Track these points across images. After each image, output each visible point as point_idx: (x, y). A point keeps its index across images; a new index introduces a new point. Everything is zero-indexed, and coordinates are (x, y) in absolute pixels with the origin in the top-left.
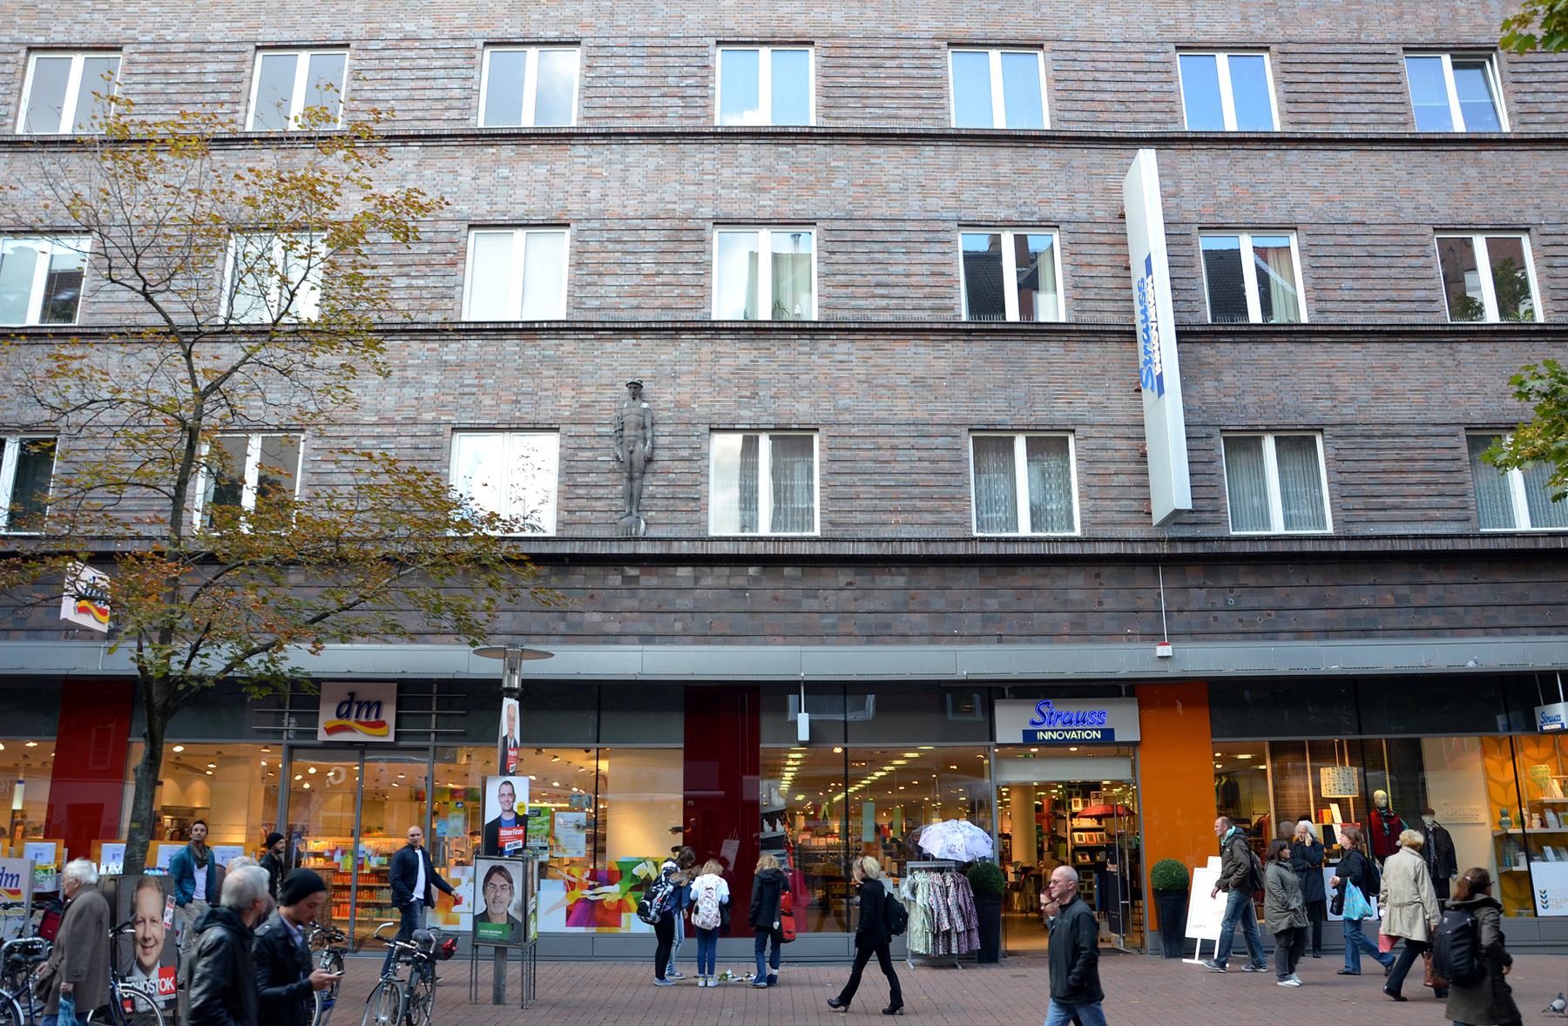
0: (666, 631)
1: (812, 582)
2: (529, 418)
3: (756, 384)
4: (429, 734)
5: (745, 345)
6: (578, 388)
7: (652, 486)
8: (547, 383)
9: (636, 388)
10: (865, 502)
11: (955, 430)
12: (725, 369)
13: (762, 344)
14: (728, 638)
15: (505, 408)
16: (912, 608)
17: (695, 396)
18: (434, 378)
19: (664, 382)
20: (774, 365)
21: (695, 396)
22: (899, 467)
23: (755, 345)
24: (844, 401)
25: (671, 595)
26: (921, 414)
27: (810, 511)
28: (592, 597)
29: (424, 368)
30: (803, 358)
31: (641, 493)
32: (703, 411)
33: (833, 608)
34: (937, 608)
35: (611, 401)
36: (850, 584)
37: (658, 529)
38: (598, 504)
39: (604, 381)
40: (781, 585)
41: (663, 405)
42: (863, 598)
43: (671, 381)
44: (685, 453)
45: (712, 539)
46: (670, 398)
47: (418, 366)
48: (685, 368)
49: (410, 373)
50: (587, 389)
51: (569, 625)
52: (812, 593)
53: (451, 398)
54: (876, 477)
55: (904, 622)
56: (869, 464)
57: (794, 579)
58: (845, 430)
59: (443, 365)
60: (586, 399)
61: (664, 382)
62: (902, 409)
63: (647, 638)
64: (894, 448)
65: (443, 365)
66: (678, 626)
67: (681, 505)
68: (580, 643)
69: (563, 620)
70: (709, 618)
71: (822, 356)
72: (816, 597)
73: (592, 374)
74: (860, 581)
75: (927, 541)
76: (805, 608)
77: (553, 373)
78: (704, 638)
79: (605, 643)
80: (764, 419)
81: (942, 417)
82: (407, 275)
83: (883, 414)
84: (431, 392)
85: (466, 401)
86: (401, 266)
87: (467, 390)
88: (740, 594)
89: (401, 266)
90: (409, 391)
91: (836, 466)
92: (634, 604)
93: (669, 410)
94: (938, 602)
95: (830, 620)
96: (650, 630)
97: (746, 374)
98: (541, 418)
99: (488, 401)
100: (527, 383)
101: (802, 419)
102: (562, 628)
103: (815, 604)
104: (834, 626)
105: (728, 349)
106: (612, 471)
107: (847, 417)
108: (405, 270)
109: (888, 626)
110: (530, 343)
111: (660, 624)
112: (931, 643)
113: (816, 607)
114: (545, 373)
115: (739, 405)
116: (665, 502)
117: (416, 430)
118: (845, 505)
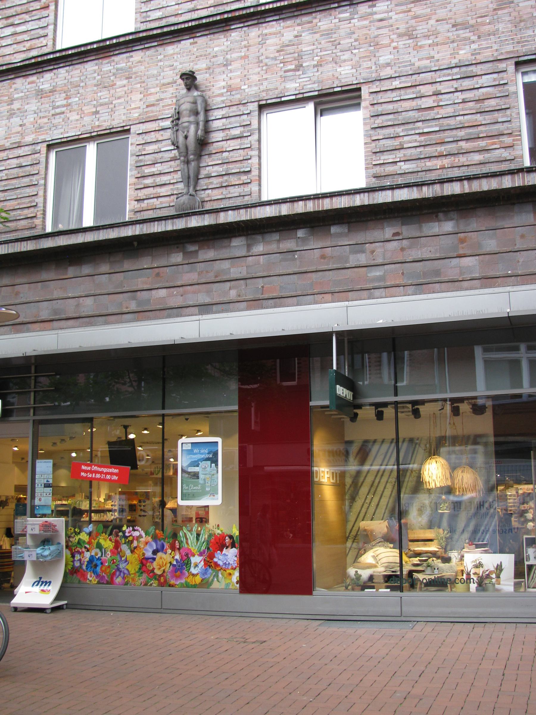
0: (222, 299)
1: (360, 237)
2: (106, 125)
3: (300, 57)
4: (28, 409)
5: (289, 23)
6: (145, 93)
7: (211, 166)
8: (120, 92)
9: (189, 79)
10: (409, 152)
11: (502, 66)
12: (272, 48)
13: (305, 19)
14: (278, 300)
15: (87, 119)
16: (461, 252)
17: (245, 78)
18: (33, 106)
19: (217, 70)
20: (317, 36)
21: (245, 78)
22: (443, 112)
23: (298, 21)
24: (385, 57)
25: (226, 265)
26: (464, 54)
27: (295, 374)
28: (158, 275)
29: (25, 99)
30: (345, 26)
31: (198, 173)
32: (254, 90)
33: (380, 261)
34: (488, 250)
35: (171, 95)
36: (397, 234)
37: (221, 198)
38: (163, 191)
39: (166, 81)
40: (328, 244)
41: (218, 92)
42: (410, 248)
43: (223, 69)
44: (236, 132)
45: (269, 203)
46: (223, 84)
47: (21, 98)
48: (235, 55)
49: (16, 105)
50: (153, 90)
51: (139, 304)
52: (358, 248)
53: (46, 120)
54: (419, 124)
55: (453, 268)
56: (411, 114)
57: (340, 235)
58: (387, 85)
59: (40, 94)
60: (152, 99)
61: (217, 70)
62: (444, 56)
63: (205, 308)
64: (437, 94)
65: (40, 94)
66: (233, 294)
67: (234, 180)
68: (149, 319)
69: (134, 298)
70: (260, 283)
71: (362, 18)
72: (363, 251)
73: (156, 77)
74: (407, 230)
75: (469, 178)
76: (351, 264)
77: (125, 82)
78: (256, 302)
79: (169, 316)
80: (309, 87)
81: (487, 55)
82: (13, 25)
83: (426, 63)
84: (31, 118)
85: (58, 120)
86: (8, 18)
87: (58, 111)
88: (289, 256)
89: (8, 18)
90: (16, 121)
91: (379, 121)
92: (193, 277)
93: (222, 95)
94: (491, 244)
95: (377, 273)
96: (207, 300)
97: (290, 49)
98: (115, 123)
99: (74, 117)
100: (104, 95)
101: (344, 81)
102: (133, 306)
103: (362, 259)
104: (382, 278)
105: (273, 30)
106: (174, 159)
107: (388, 72)
108: (10, 21)
109: (437, 272)
110: (106, 61)
111: (218, 292)
112: (482, 287)
113: (363, 262)
114: (119, 83)
115: (284, 79)
116: (220, 180)
117: (21, 152)
118: (389, 157)
